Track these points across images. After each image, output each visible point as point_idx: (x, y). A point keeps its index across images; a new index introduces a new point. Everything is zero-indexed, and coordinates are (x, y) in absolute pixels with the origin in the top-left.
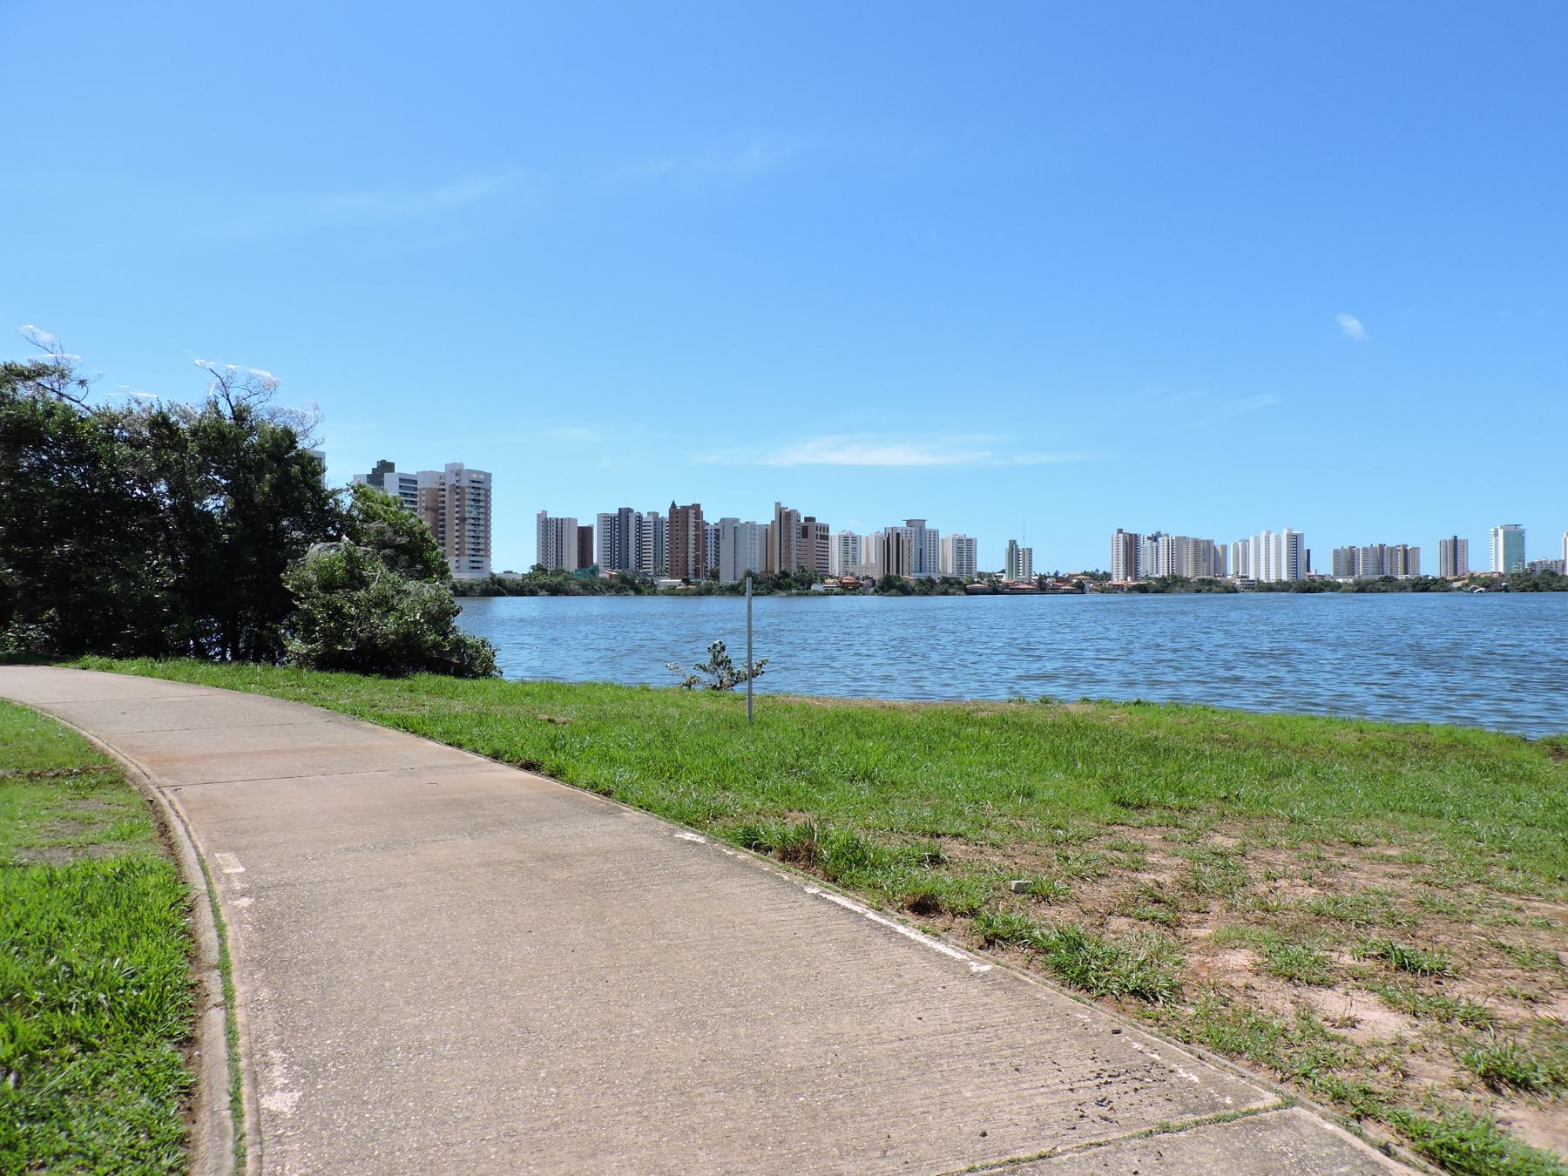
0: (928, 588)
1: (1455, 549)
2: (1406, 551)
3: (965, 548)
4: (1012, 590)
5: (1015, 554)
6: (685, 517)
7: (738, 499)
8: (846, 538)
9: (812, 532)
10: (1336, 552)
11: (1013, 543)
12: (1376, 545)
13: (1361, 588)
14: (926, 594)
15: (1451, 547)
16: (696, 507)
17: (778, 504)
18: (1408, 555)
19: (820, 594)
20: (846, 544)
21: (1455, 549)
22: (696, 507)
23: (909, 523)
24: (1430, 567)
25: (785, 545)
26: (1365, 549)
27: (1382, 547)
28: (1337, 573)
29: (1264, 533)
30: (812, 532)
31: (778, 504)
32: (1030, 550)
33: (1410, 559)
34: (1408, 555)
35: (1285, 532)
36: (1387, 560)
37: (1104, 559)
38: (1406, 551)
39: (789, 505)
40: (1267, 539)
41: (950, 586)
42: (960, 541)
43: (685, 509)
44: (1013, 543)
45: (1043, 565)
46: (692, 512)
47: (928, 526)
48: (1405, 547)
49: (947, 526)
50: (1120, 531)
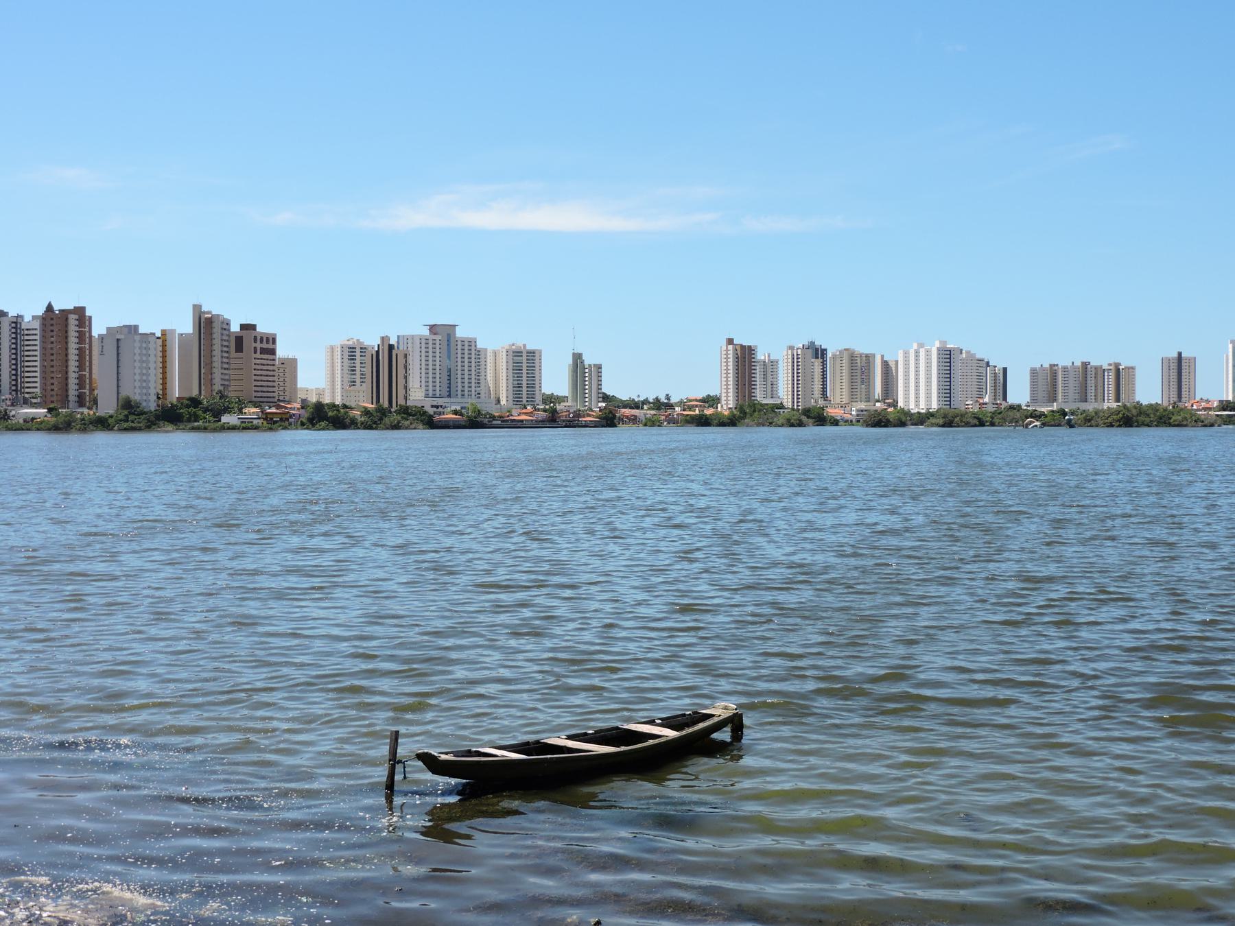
0: (475, 422)
1: (1179, 369)
2: (1118, 371)
3: (525, 364)
4: (574, 422)
5: (581, 371)
6: (63, 325)
7: (141, 297)
8: (352, 349)
9: (248, 344)
10: (1034, 372)
11: (577, 357)
12: (1046, 365)
13: (1059, 419)
14: (370, 428)
15: (1174, 366)
16: (80, 311)
17: (197, 308)
18: (1121, 375)
19: (234, 428)
20: (352, 357)
21: (1179, 369)
22: (80, 311)
23: (433, 329)
24: (1149, 390)
25: (205, 361)
26: (1065, 368)
27: (1085, 365)
28: (1034, 399)
29: (915, 346)
30: (253, 345)
31: (197, 308)
32: (599, 367)
33: (1122, 382)
34: (1121, 375)
35: (937, 344)
36: (1091, 382)
37: (709, 379)
38: (1118, 371)
39: (212, 307)
40: (917, 352)
41: (1160, 418)
42: (518, 353)
43: (65, 313)
44: (577, 357)
45: (618, 386)
46: (72, 320)
47: (460, 333)
48: (1117, 366)
49: (492, 335)
50: (730, 341)
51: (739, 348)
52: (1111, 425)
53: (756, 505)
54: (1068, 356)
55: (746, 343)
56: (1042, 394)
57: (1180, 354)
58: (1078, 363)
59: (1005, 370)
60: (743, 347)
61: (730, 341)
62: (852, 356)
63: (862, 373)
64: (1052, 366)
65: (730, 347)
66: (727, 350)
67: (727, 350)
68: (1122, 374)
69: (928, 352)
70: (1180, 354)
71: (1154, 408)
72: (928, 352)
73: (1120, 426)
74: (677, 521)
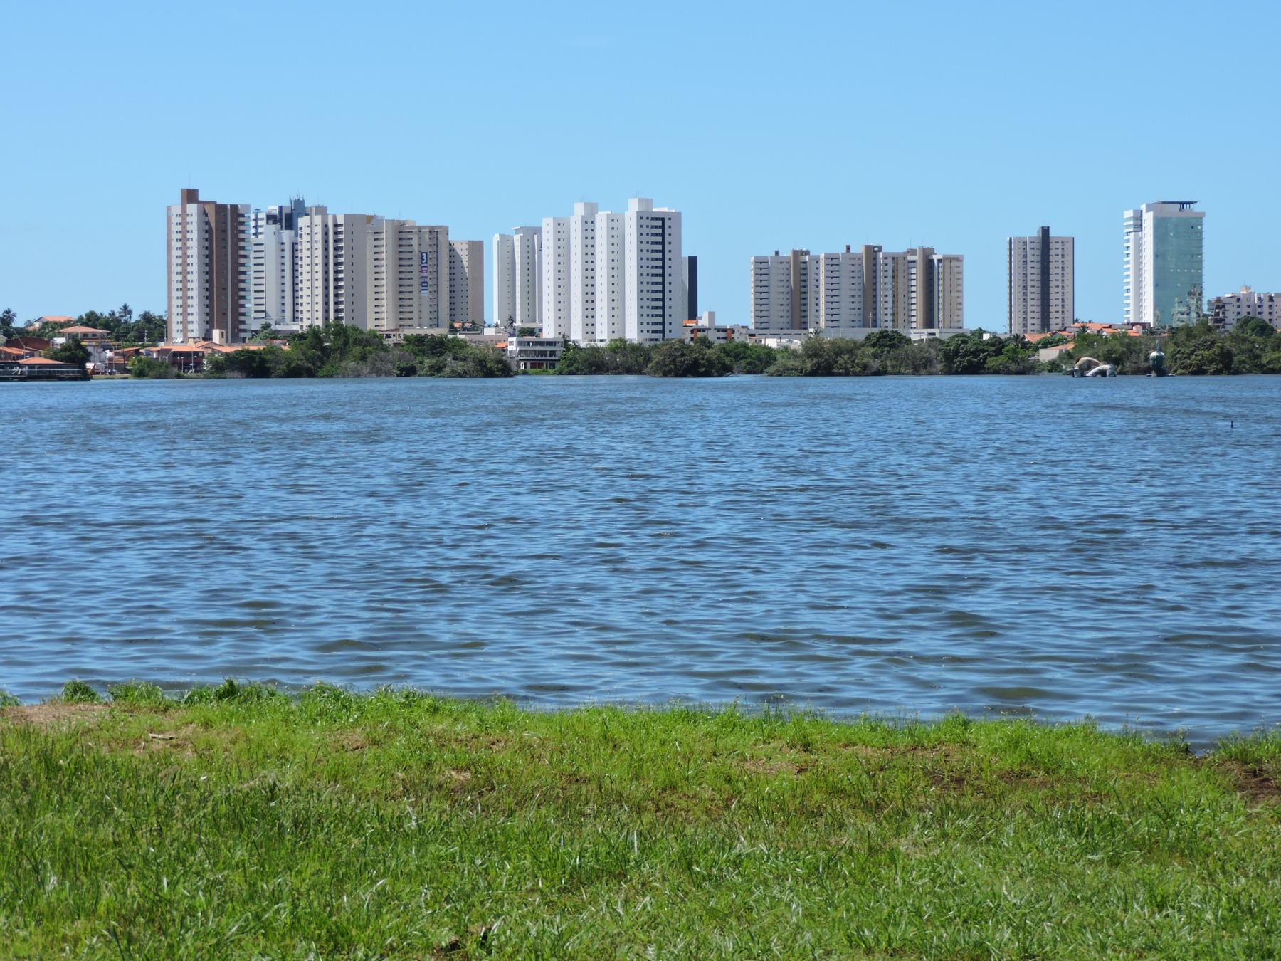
1: (1044, 260)
2: (929, 265)
10: (761, 266)
12: (786, 253)
13: (823, 363)
15: (1033, 256)
18: (934, 274)
21: (1044, 260)
24: (986, 309)
26: (831, 258)
27: (872, 252)
28: (763, 323)
29: (579, 210)
34: (934, 274)
37: (147, 277)
38: (929, 265)
40: (588, 225)
48: (927, 254)
51: (211, 211)
52: (1199, 371)
53: (1154, 576)
54: (829, 234)
55: (226, 199)
56: (778, 310)
57: (1045, 231)
58: (858, 249)
59: (693, 261)
60: (220, 209)
61: (190, 196)
62: (402, 232)
63: (423, 267)
64: (797, 254)
65: (192, 208)
66: (184, 214)
67: (184, 214)
68: (940, 271)
69: (615, 224)
70: (1045, 231)
71: (998, 345)
72: (615, 224)
73: (1217, 372)
74: (38, 622)
